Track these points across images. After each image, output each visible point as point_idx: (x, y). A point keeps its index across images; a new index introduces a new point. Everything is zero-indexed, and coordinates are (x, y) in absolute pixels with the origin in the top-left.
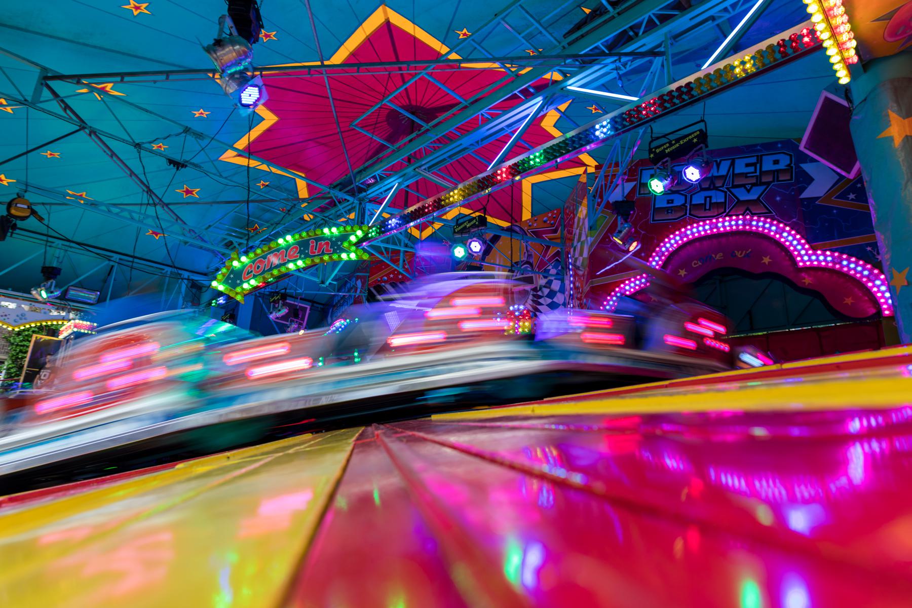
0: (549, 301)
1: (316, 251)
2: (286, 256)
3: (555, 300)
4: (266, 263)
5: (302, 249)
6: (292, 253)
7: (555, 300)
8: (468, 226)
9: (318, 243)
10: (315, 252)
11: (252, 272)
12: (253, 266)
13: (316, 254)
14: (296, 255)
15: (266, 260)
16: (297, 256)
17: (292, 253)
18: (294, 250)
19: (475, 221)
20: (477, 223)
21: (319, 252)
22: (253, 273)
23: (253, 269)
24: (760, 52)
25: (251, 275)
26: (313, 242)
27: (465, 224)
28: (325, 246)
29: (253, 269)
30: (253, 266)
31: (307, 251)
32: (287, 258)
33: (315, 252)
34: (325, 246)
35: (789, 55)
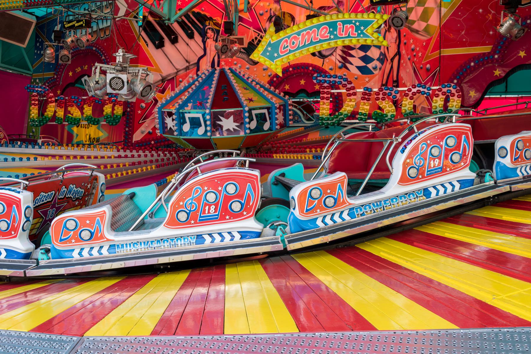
0: (362, 54)
1: (344, 33)
2: (318, 36)
3: (369, 53)
4: (300, 39)
5: (331, 29)
6: (323, 33)
7: (369, 53)
8: (76, 25)
9: (345, 25)
10: (342, 35)
11: (287, 46)
12: (289, 41)
13: (344, 36)
14: (326, 35)
15: (300, 37)
16: (327, 36)
17: (323, 33)
18: (325, 30)
19: (82, 23)
20: (84, 25)
21: (345, 34)
22: (289, 48)
23: (288, 44)
24: (418, 125)
25: (287, 51)
26: (340, 25)
27: (74, 23)
28: (350, 30)
29: (288, 44)
30: (289, 41)
31: (335, 33)
32: (319, 37)
33: (342, 35)
34: (350, 30)
35: (504, 17)
